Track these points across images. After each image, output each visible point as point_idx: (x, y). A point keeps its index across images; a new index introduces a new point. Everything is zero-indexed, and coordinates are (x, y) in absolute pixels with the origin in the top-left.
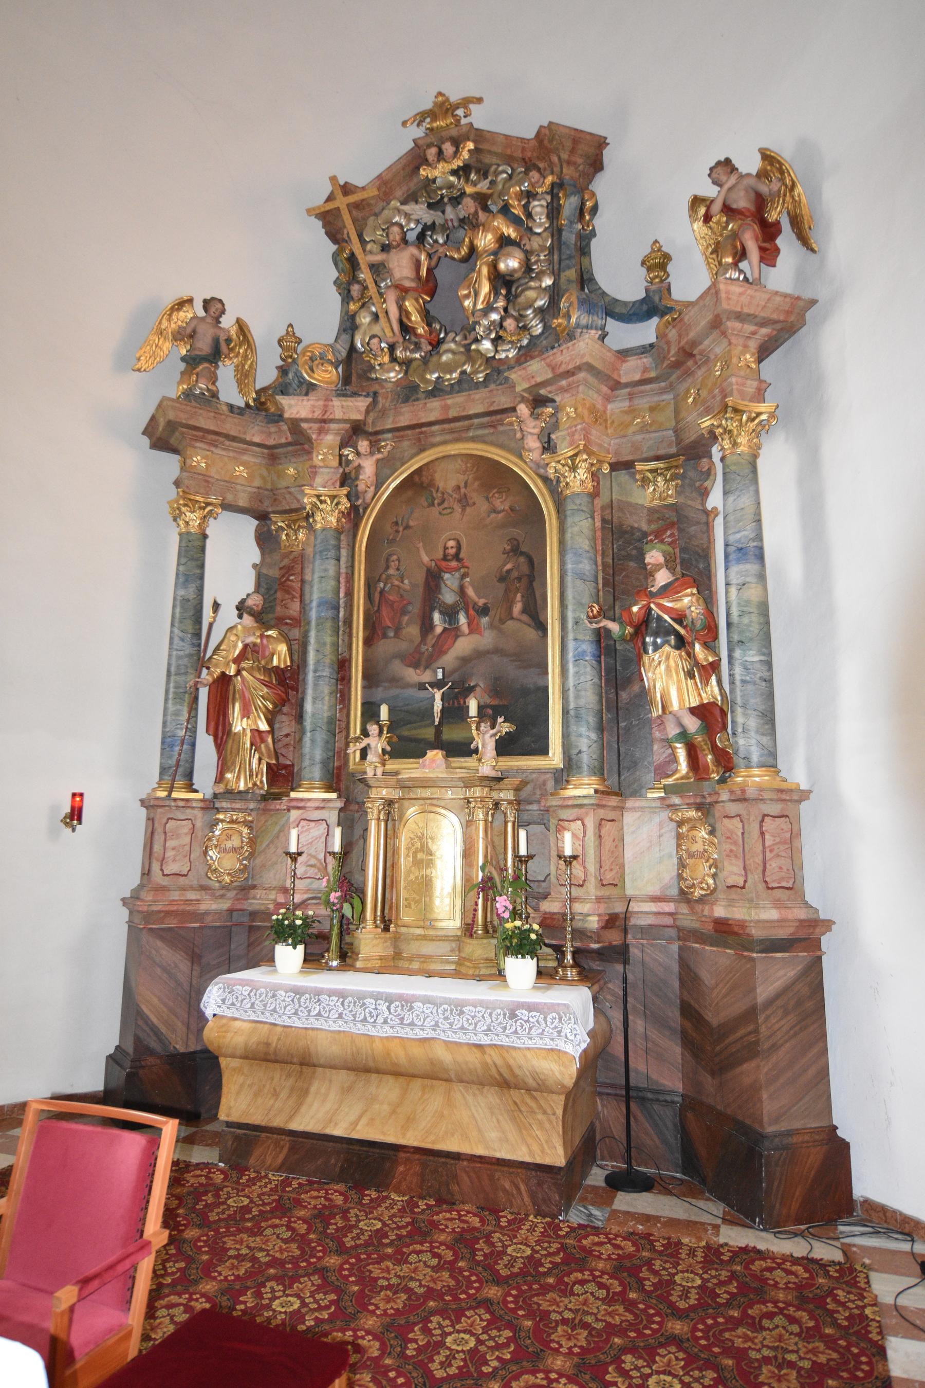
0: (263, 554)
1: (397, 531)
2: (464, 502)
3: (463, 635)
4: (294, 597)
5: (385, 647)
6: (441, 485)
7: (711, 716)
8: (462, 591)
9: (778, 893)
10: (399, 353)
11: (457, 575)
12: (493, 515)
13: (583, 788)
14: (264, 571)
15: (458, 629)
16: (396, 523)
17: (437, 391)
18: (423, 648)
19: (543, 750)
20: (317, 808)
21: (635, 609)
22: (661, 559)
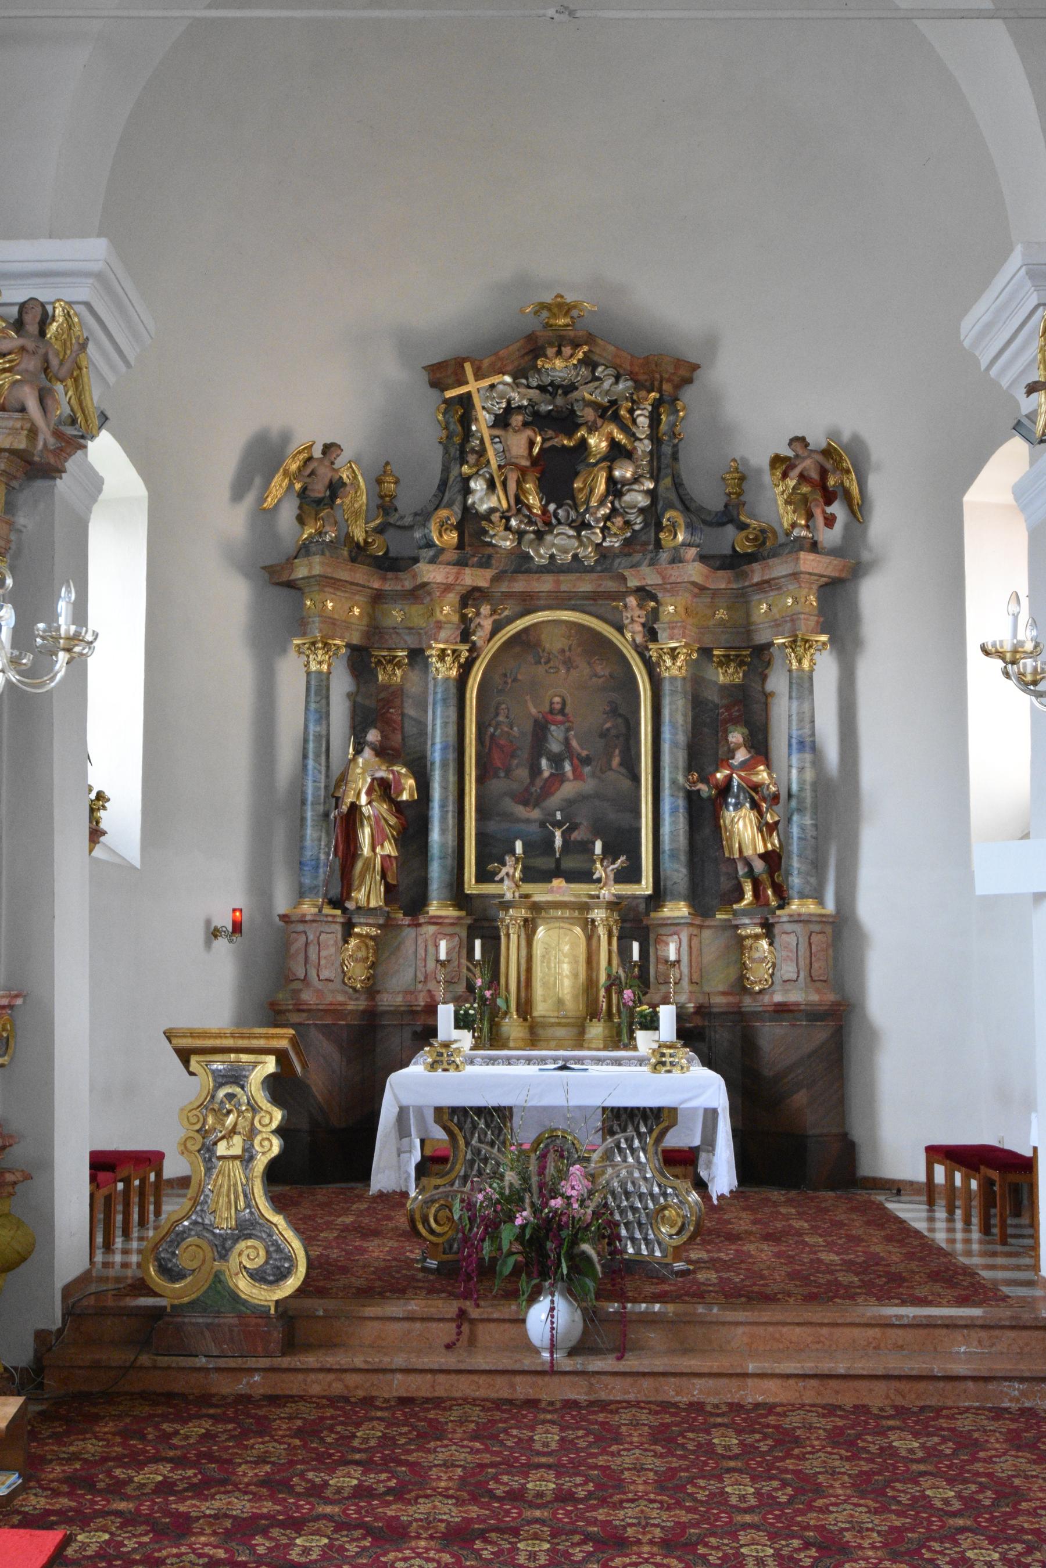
0: (358, 685)
1: (506, 683)
2: (569, 664)
3: (568, 780)
4: (395, 729)
5: (497, 785)
6: (548, 646)
7: (773, 859)
8: (567, 742)
9: (819, 985)
10: (513, 522)
11: (562, 728)
12: (594, 679)
13: (677, 910)
14: (359, 699)
15: (563, 774)
16: (505, 675)
17: (552, 567)
18: (533, 789)
19: (638, 881)
20: (452, 924)
21: (719, 775)
22: (741, 740)
